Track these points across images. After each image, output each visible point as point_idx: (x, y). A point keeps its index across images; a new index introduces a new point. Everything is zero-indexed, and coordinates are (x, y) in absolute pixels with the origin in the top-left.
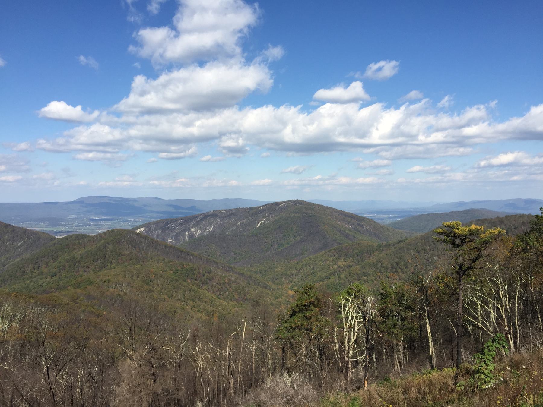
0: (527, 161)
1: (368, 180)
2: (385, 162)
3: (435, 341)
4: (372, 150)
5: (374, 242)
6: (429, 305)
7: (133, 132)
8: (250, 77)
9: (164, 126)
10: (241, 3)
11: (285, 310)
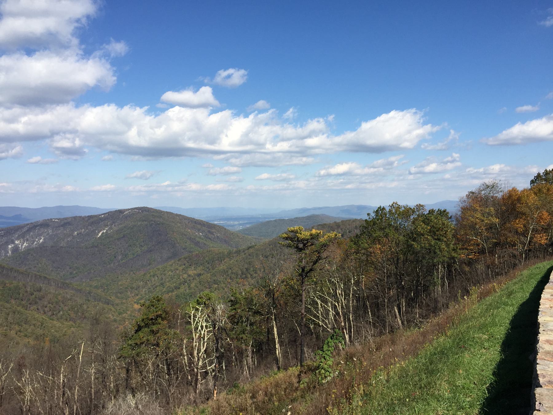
0: (359, 171)
1: (218, 187)
2: (235, 169)
4: (222, 156)
5: (224, 249)
11: (129, 326)
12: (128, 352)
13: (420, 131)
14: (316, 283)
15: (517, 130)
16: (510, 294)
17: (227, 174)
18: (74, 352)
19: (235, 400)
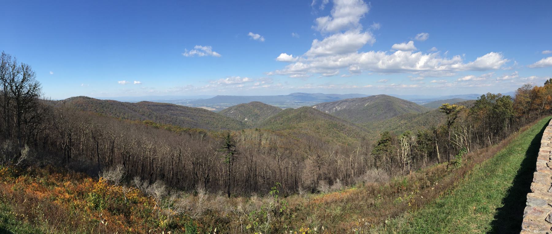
0: (475, 79)
1: (414, 86)
2: (422, 78)
3: (440, 153)
4: (417, 73)
5: (416, 113)
6: (437, 138)
7: (312, 65)
8: (363, 38)
9: (325, 61)
10: (362, 2)
11: (375, 142)
12: (375, 152)
13: (502, 62)
14: (455, 128)
15: (542, 61)
16: (532, 131)
17: (419, 80)
18: (355, 150)
19: (419, 175)
